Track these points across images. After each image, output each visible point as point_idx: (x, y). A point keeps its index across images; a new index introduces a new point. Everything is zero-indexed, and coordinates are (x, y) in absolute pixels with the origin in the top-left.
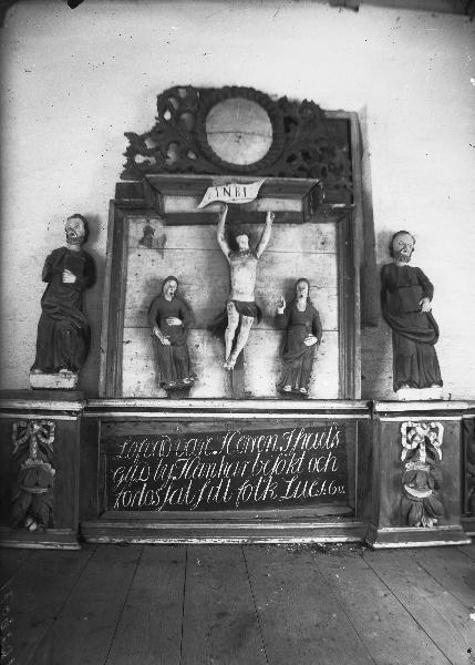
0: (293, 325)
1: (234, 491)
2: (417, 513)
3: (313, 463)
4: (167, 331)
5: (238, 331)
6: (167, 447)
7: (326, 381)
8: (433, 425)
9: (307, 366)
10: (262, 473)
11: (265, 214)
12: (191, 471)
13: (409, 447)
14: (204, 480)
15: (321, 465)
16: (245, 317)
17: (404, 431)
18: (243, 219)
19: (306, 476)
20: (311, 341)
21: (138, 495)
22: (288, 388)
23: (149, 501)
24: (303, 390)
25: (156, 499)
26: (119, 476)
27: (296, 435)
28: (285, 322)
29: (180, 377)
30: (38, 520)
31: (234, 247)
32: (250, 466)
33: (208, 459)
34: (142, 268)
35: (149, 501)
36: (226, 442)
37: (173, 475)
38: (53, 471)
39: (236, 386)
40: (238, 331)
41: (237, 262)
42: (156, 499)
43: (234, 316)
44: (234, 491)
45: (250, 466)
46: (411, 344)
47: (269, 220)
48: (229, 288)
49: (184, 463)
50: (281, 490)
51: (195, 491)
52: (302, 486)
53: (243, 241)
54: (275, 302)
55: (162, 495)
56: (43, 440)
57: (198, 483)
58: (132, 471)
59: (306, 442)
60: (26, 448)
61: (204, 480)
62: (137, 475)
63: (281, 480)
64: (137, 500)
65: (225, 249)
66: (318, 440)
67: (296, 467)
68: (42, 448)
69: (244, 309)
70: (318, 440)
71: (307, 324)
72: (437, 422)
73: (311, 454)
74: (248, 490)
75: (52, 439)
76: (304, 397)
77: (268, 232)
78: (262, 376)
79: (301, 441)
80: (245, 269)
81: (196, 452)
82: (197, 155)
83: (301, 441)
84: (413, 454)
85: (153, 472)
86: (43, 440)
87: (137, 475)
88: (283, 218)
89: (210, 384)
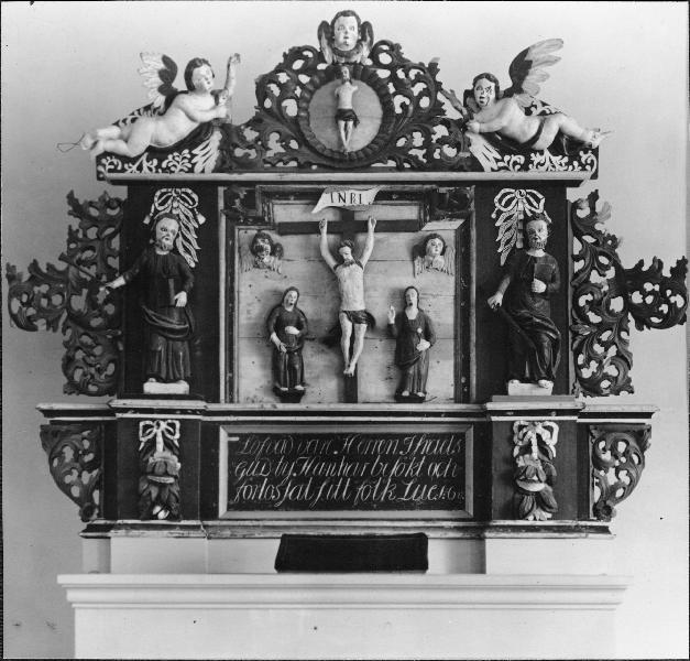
0: (403, 337)
1: (352, 489)
2: (528, 503)
3: (433, 467)
4: (283, 336)
5: (353, 339)
6: (289, 445)
7: (440, 379)
8: (548, 424)
9: (423, 372)
10: (381, 474)
11: (366, 222)
12: (311, 470)
13: (520, 444)
14: (323, 478)
15: (441, 470)
16: (357, 325)
17: (515, 429)
18: (348, 226)
19: (425, 479)
20: (424, 345)
21: (260, 489)
22: (406, 393)
23: (269, 495)
24: (421, 394)
25: (275, 493)
26: (240, 471)
27: (416, 441)
28: (395, 331)
29: (293, 383)
30: (166, 507)
31: (341, 261)
32: (369, 468)
33: (330, 459)
34: (251, 291)
35: (269, 495)
36: (348, 444)
37: (293, 471)
38: (179, 465)
39: (349, 389)
40: (353, 339)
41: (344, 272)
42: (275, 493)
43: (347, 325)
44: (352, 489)
45: (369, 468)
46: (161, 340)
47: (371, 227)
48: (339, 297)
49: (305, 461)
50: (400, 492)
51: (314, 490)
52: (421, 489)
53: (347, 252)
54: (386, 313)
55: (282, 490)
56: (169, 436)
57: (318, 481)
58: (254, 466)
59: (427, 448)
60: (152, 444)
61: (323, 478)
62: (259, 470)
63: (400, 482)
64: (257, 494)
65: (332, 262)
66: (440, 446)
67: (415, 470)
68: (168, 445)
69: (355, 318)
70: (440, 446)
71: (420, 330)
72: (551, 420)
73: (431, 459)
74: (367, 491)
75: (177, 436)
76: (421, 400)
77: (371, 239)
78: (375, 387)
79: (421, 448)
80: (523, 115)
81: (318, 451)
82: (300, 145)
83: (421, 448)
84: (527, 449)
85: (274, 466)
86: (169, 436)
87: (259, 470)
88: (387, 226)
89: (321, 392)
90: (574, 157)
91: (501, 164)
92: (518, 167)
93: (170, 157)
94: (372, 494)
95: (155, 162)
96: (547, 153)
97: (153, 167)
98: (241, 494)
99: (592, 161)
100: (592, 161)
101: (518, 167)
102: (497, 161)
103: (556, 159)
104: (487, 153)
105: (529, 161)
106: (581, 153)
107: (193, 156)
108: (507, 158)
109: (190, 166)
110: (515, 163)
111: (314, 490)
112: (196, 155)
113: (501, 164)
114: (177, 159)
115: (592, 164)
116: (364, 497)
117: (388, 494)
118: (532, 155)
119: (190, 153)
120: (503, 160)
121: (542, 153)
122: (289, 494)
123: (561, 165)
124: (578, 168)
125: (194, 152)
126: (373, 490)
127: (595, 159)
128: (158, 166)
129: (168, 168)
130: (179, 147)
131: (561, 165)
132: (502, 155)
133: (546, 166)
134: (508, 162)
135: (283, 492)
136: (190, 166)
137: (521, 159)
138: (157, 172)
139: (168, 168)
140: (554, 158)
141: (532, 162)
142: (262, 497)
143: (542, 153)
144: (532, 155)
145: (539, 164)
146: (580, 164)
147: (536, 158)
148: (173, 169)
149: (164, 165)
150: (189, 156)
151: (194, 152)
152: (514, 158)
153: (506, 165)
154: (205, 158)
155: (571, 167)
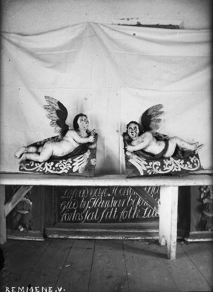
23: (77, 218)
35: (77, 218)
50: (142, 214)
51: (99, 215)
64: (72, 218)
90: (187, 160)
91: (148, 167)
92: (158, 168)
93: (61, 162)
94: (128, 215)
95: (52, 163)
96: (172, 159)
97: (50, 166)
98: (122, 216)
99: (197, 161)
100: (197, 161)
101: (158, 168)
102: (145, 165)
103: (178, 162)
104: (139, 162)
105: (163, 164)
106: (190, 158)
107: (74, 162)
108: (150, 164)
109: (71, 167)
110: (156, 166)
111: (99, 215)
112: (75, 162)
113: (148, 167)
114: (64, 163)
115: (197, 162)
116: (124, 217)
117: (136, 215)
118: (164, 160)
119: (72, 160)
120: (148, 165)
121: (169, 159)
122: (87, 217)
123: (180, 164)
124: (190, 166)
125: (74, 160)
126: (128, 213)
127: (198, 160)
128: (53, 166)
129: (59, 167)
130: (66, 157)
131: (180, 164)
132: (148, 163)
133: (172, 166)
134: (152, 166)
135: (84, 217)
136: (71, 167)
137: (158, 163)
138: (52, 169)
139: (59, 167)
140: (176, 161)
141: (165, 164)
142: (74, 218)
143: (169, 160)
144: (164, 160)
145: (169, 165)
146: (191, 163)
147: (167, 162)
148: (61, 168)
149: (57, 165)
150: (71, 162)
151: (74, 160)
152: (156, 163)
153: (151, 167)
154: (79, 164)
155: (186, 165)
